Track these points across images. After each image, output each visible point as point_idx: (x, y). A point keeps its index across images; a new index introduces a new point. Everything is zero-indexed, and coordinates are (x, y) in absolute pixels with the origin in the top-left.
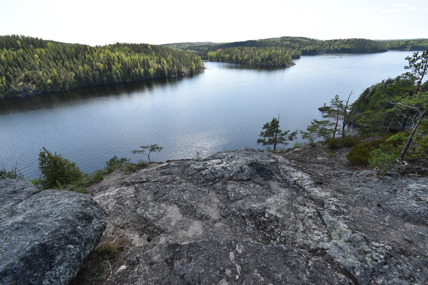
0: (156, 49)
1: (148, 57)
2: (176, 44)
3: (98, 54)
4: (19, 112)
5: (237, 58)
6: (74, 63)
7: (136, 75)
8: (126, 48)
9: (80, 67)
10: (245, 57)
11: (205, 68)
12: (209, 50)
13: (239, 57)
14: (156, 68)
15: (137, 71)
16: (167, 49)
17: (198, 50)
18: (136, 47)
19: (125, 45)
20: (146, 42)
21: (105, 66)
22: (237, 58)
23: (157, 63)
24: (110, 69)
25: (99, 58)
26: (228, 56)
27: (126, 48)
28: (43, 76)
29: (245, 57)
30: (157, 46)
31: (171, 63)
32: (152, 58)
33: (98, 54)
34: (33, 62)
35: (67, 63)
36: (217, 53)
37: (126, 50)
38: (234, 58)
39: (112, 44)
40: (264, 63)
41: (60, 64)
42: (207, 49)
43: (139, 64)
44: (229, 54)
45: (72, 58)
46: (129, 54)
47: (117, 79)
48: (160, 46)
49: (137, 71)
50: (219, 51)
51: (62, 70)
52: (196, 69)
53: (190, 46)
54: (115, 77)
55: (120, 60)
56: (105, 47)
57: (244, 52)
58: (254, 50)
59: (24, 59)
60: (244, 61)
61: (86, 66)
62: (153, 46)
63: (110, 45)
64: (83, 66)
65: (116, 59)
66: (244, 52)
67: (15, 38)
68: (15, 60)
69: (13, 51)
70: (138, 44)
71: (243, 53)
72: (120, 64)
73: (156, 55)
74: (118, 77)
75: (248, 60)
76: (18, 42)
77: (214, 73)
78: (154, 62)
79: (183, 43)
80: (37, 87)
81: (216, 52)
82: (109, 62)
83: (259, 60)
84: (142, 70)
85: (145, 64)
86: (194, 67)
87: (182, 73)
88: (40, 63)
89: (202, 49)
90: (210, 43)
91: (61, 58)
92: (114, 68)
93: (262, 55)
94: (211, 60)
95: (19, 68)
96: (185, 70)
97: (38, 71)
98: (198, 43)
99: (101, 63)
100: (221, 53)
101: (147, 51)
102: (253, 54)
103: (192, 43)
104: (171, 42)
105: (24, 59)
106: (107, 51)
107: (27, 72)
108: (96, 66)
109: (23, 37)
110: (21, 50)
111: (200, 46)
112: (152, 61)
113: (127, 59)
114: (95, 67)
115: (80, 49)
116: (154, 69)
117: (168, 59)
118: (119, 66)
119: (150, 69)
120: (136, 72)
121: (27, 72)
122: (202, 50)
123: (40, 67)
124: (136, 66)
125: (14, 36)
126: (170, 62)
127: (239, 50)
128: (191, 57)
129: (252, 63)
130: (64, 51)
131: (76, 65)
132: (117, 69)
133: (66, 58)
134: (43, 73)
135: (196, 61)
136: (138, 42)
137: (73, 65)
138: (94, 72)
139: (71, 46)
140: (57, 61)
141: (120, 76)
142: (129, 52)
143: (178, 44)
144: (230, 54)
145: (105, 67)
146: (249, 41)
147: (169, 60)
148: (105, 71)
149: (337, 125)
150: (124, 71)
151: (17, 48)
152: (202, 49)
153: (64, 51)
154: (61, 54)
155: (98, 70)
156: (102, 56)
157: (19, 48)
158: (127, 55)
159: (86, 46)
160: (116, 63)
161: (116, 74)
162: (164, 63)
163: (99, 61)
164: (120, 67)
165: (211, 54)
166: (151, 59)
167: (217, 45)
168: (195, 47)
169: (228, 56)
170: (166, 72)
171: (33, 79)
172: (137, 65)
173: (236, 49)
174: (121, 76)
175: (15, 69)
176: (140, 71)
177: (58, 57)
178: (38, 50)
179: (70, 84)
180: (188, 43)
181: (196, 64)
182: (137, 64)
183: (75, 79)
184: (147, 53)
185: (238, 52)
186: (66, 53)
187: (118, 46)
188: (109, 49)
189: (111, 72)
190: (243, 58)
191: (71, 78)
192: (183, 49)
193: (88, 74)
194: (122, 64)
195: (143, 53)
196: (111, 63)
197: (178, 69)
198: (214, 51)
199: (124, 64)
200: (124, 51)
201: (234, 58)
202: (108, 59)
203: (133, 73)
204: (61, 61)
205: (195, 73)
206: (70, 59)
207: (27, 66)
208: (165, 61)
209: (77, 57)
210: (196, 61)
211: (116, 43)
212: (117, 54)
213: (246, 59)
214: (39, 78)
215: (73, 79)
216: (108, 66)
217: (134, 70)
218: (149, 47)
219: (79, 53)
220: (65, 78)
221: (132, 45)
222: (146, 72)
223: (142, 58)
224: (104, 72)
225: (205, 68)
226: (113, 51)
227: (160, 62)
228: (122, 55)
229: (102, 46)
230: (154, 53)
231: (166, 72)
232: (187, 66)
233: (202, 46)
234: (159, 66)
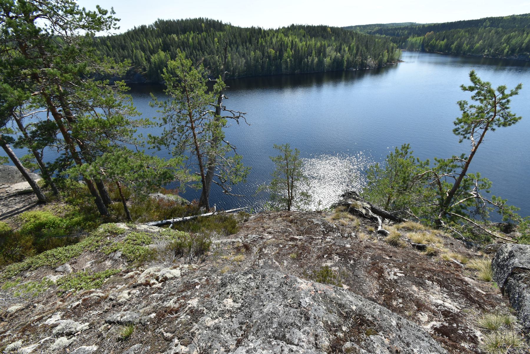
0: (335, 31)
1: (326, 43)
2: (360, 26)
3: (271, 39)
4: (516, 70)
5: (459, 46)
6: (247, 49)
7: (308, 66)
8: (301, 31)
9: (252, 53)
10: (478, 45)
11: (402, 61)
12: (409, 34)
13: (465, 45)
14: (333, 57)
15: (310, 60)
16: (351, 32)
17: (393, 34)
18: (313, 30)
19: (301, 27)
20: (324, 24)
21: (276, 52)
22: (459, 46)
23: (336, 50)
24: (281, 56)
25: (272, 43)
26: (443, 43)
27: (301, 31)
28: (219, 61)
29: (478, 45)
30: (338, 28)
31: (355, 51)
32: (331, 44)
33: (271, 39)
34: (212, 46)
35: (240, 48)
36: (424, 39)
37: (300, 34)
38: (453, 46)
39: (286, 27)
40: (515, 57)
41: (234, 49)
42: (406, 32)
43: (314, 52)
44: (445, 40)
45: (246, 43)
46: (303, 39)
47: (286, 69)
48: (342, 29)
49: (310, 60)
50: (428, 36)
51: (235, 56)
52: (388, 61)
53: (381, 30)
54: (284, 66)
55: (293, 46)
56: (278, 31)
57: (476, 37)
58: (497, 33)
59: (206, 42)
60: (473, 52)
61: (258, 52)
62: (332, 29)
63: (284, 28)
64: (255, 51)
65: (290, 44)
66: (476, 37)
67: (201, 20)
68: (199, 43)
69: (198, 34)
70: (315, 26)
71: (474, 38)
72: (293, 51)
73: (335, 40)
74: (287, 67)
75: (482, 50)
76: (203, 25)
77: (413, 71)
78: (332, 49)
79: (370, 25)
80: (212, 72)
81: (422, 37)
82: (281, 48)
83: (506, 51)
84: (316, 60)
85: (321, 52)
86: (385, 59)
87: (366, 66)
88: (218, 48)
89: (398, 33)
90: (412, 24)
91: (236, 42)
92: (285, 55)
93: (514, 41)
94: (412, 49)
95: (201, 52)
96: (371, 62)
97: (215, 56)
98: (393, 24)
99: (273, 49)
100: (432, 38)
101: (326, 34)
102: (495, 40)
103: (383, 25)
104: (354, 25)
105: (206, 42)
106: (281, 35)
107: (207, 56)
108: (267, 52)
109: (207, 20)
110: (204, 34)
111: (396, 29)
112: (330, 48)
113: (301, 44)
114: (266, 54)
115: (255, 33)
116: (330, 59)
117: (351, 45)
118: (291, 53)
119: (325, 58)
120: (308, 61)
121: (207, 56)
122: (398, 35)
123: (217, 51)
124: (310, 54)
125: (200, 19)
126: (353, 50)
127: (467, 34)
128: (385, 43)
129: (487, 55)
130: (240, 35)
131: (248, 51)
132: (288, 57)
133: (240, 43)
134: (219, 58)
135: (390, 49)
136: (315, 22)
137: (245, 50)
138: (264, 59)
139: (247, 30)
140: (232, 46)
141: (289, 66)
142: (304, 36)
143: (363, 26)
144: (448, 40)
145: (276, 55)
146: (487, 18)
147: (353, 47)
148: (275, 58)
149: (439, 183)
150: (295, 60)
151: (200, 31)
152: (398, 33)
153: (240, 35)
154: (237, 37)
155: (269, 57)
156: (274, 40)
157: (202, 32)
158: (301, 40)
159: (260, 29)
160: (289, 49)
161: (286, 62)
162: (344, 51)
163: (271, 46)
164: (292, 55)
165: (412, 39)
166: (329, 46)
167: (426, 26)
168: (389, 30)
169: (443, 43)
170: (345, 63)
171: (210, 64)
172: (312, 53)
173: (462, 32)
174: (291, 66)
175: (198, 53)
176: (313, 60)
177: (234, 42)
178: (218, 33)
179: (239, 73)
180: (377, 24)
181: (389, 55)
182: (312, 51)
183: (245, 66)
184: (324, 38)
185: (465, 36)
186: (241, 37)
187: (293, 28)
188: (282, 32)
189: (281, 60)
190: (472, 47)
191: (241, 65)
192: (370, 33)
193: (257, 61)
194: (295, 51)
195: (320, 38)
196: (283, 49)
197: (362, 60)
198: (419, 35)
199: (297, 51)
200: (298, 35)
201: (453, 46)
202: (281, 44)
203: (304, 62)
204: (236, 46)
205: (381, 68)
206: (244, 44)
207: (208, 50)
208: (347, 49)
209: (250, 43)
210: (390, 49)
211: (291, 24)
212: (290, 38)
213: (477, 49)
214: (215, 63)
215: (243, 66)
216: (279, 53)
217: (307, 58)
218: (329, 29)
219: (253, 37)
220: (236, 65)
221: (308, 27)
222: (321, 62)
223: (319, 44)
224: (273, 60)
225: (402, 61)
226: (286, 35)
227: (340, 49)
228: (296, 40)
229: (275, 29)
230: (333, 38)
231: (345, 63)
232: (375, 57)
233: (400, 29)
234: (339, 54)
